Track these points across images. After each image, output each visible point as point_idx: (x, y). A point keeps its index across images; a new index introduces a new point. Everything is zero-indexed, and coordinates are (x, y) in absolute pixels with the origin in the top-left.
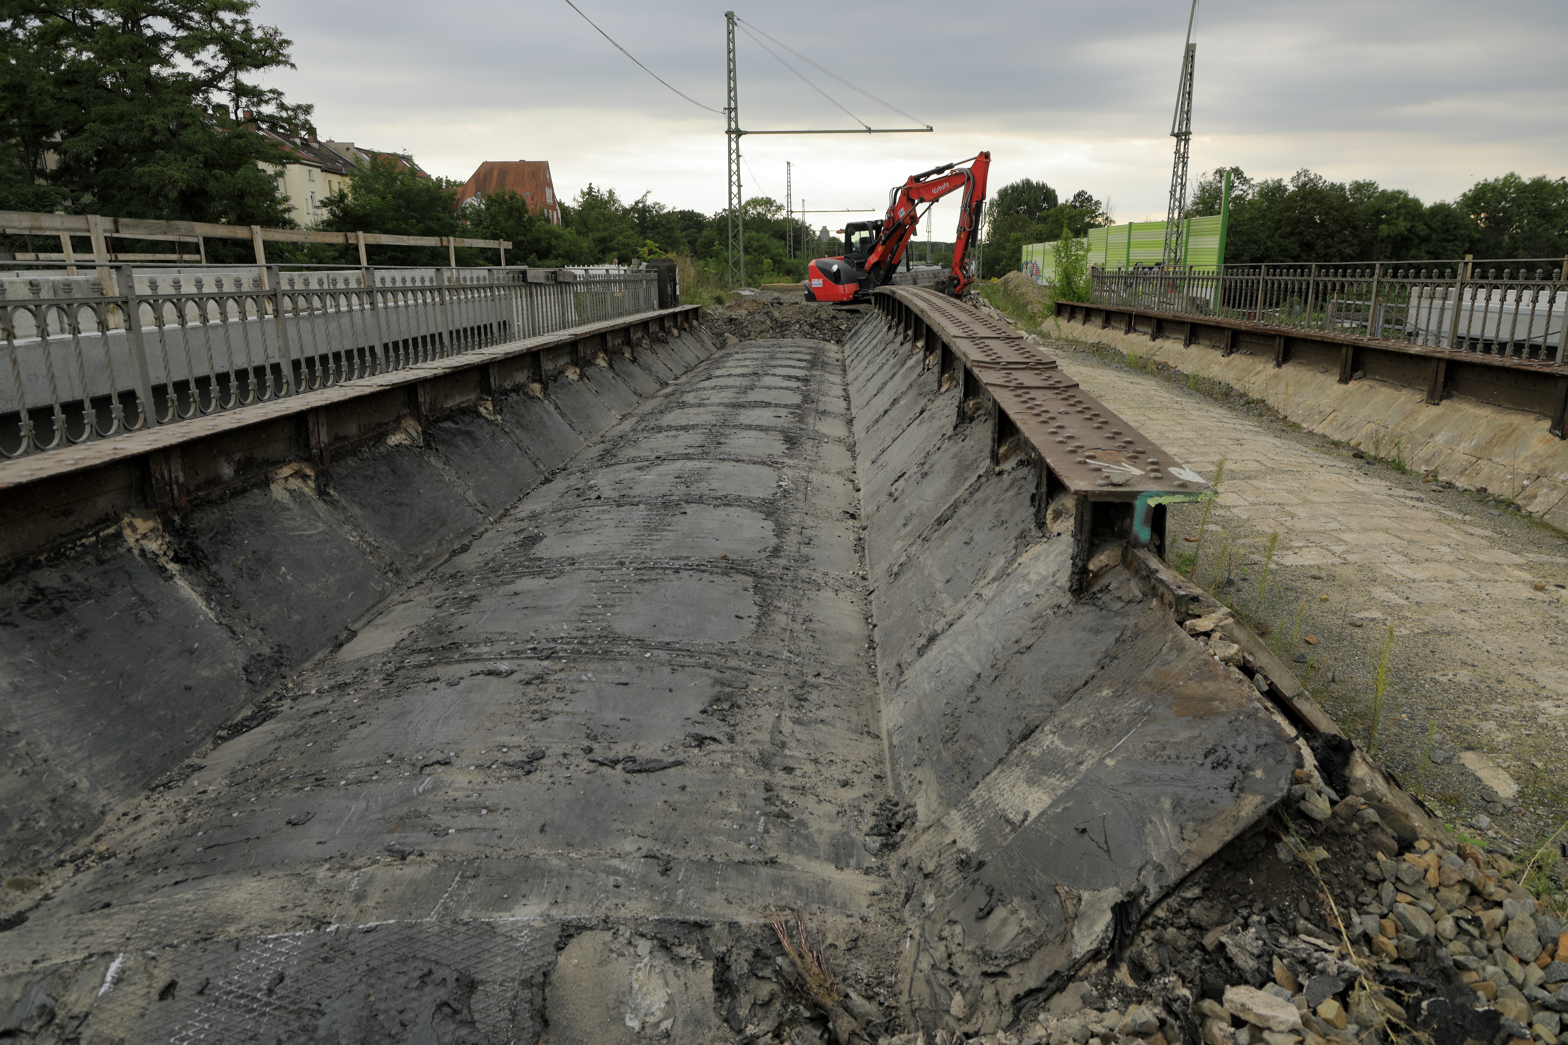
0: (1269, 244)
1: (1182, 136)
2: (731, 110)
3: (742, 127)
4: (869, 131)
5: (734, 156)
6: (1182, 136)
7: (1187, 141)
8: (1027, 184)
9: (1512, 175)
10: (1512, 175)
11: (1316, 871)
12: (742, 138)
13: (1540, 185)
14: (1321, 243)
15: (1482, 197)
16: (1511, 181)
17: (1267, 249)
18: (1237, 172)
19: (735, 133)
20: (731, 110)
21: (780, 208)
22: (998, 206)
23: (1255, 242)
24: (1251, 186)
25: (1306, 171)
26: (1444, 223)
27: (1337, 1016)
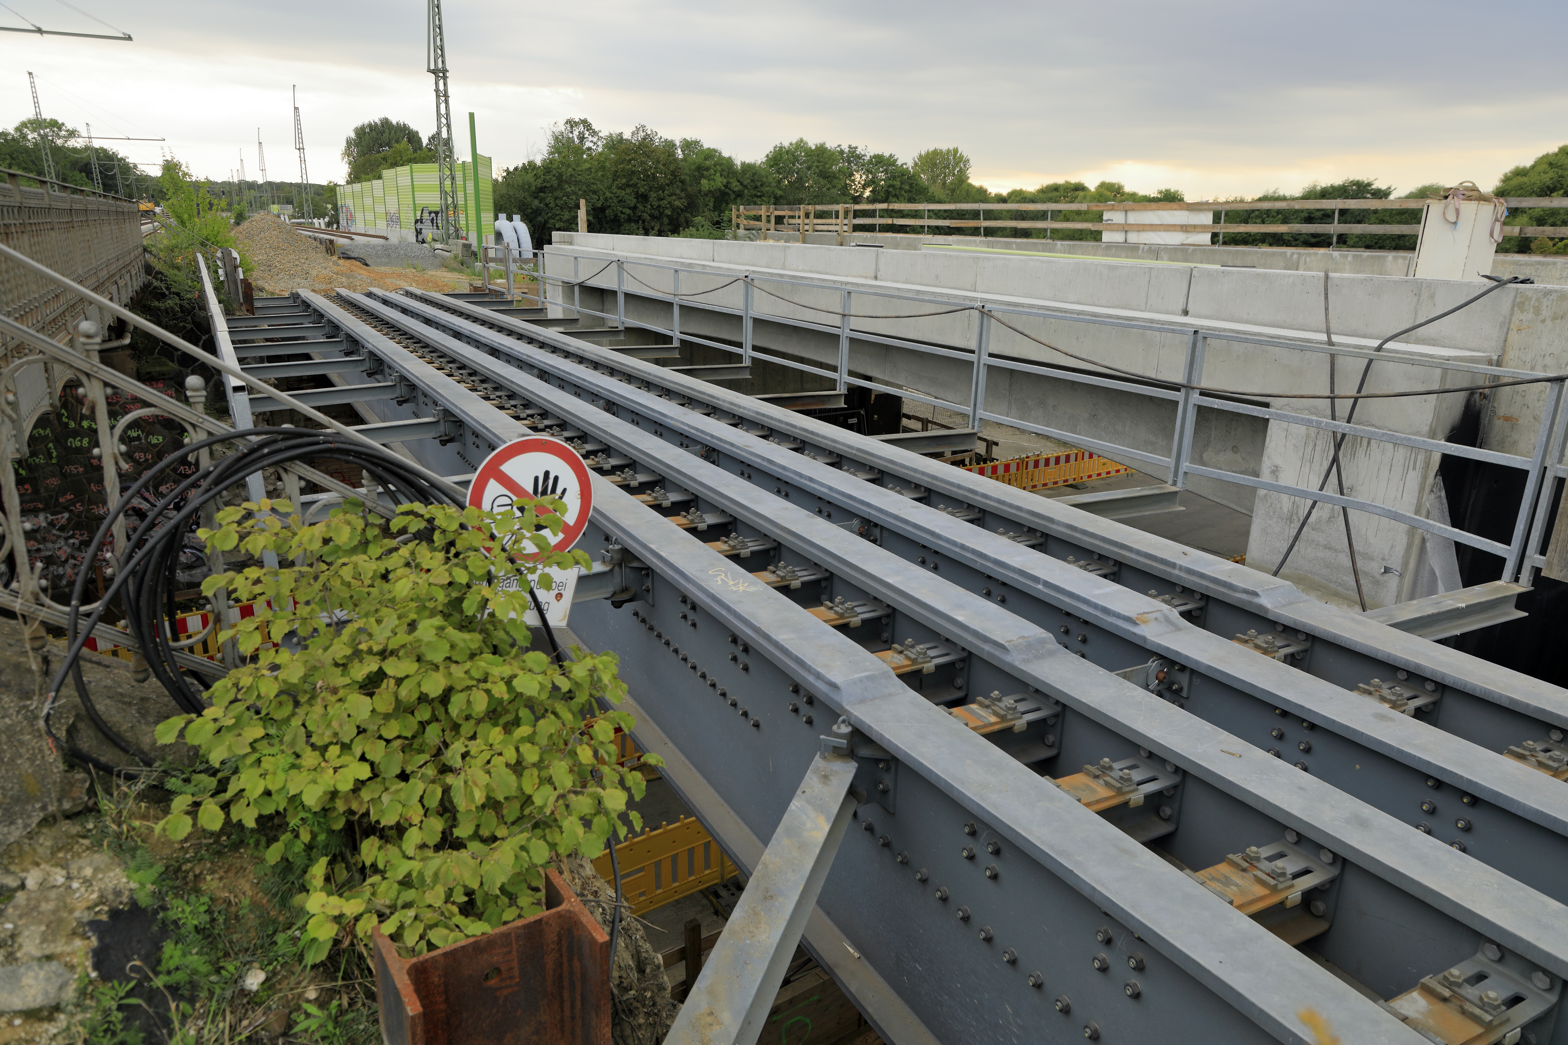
0: (608, 194)
1: (440, 73)
4: (40, 31)
6: (440, 73)
7: (445, 78)
8: (386, 122)
9: (802, 140)
10: (802, 140)
13: (821, 150)
14: (653, 195)
15: (781, 159)
16: (801, 145)
17: (606, 199)
21: (72, 134)
22: (357, 145)
23: (595, 192)
24: (600, 138)
26: (752, 181)
27: (325, 941)
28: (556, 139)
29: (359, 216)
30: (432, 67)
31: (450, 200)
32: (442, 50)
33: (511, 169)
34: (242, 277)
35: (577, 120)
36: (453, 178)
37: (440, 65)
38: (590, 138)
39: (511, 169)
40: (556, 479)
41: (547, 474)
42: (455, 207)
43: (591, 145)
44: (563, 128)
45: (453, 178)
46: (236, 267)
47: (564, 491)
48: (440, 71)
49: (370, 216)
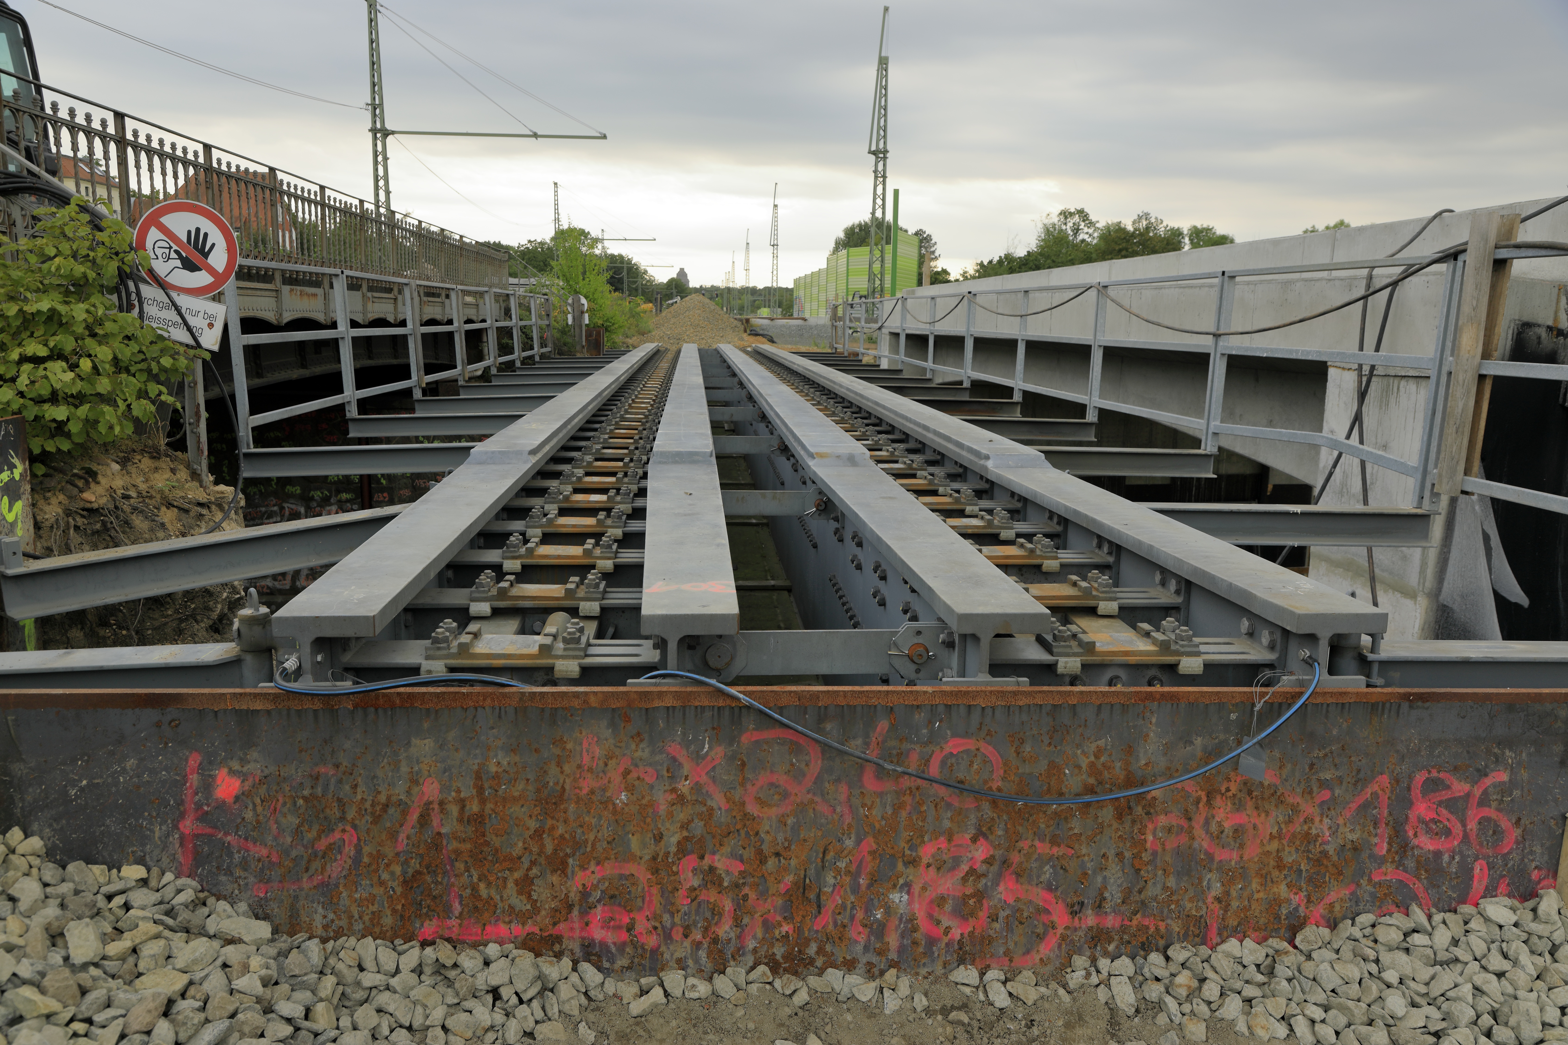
1: (880, 154)
2: (376, 108)
3: (389, 126)
4: (535, 135)
5: (380, 158)
7: (885, 158)
11: (853, 836)
12: (390, 139)
18: (1082, 214)
19: (380, 133)
20: (376, 108)
24: (1096, 229)
25: (1147, 214)
28: (1047, 231)
29: (807, 306)
30: (873, 148)
31: (878, 282)
32: (885, 131)
33: (985, 263)
34: (587, 322)
35: (1072, 210)
36: (882, 261)
37: (881, 145)
38: (1086, 230)
39: (985, 263)
40: (206, 235)
41: (198, 230)
42: (882, 290)
43: (1086, 237)
44: (1055, 220)
45: (882, 261)
46: (582, 312)
47: (213, 245)
48: (881, 152)
49: (815, 305)
